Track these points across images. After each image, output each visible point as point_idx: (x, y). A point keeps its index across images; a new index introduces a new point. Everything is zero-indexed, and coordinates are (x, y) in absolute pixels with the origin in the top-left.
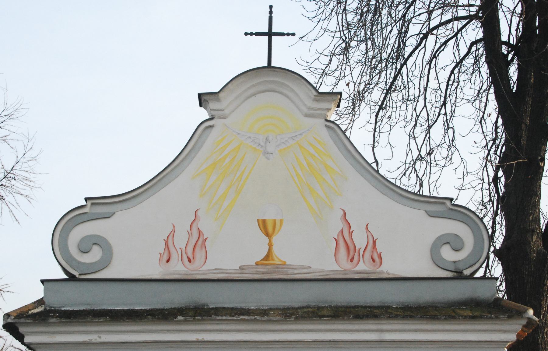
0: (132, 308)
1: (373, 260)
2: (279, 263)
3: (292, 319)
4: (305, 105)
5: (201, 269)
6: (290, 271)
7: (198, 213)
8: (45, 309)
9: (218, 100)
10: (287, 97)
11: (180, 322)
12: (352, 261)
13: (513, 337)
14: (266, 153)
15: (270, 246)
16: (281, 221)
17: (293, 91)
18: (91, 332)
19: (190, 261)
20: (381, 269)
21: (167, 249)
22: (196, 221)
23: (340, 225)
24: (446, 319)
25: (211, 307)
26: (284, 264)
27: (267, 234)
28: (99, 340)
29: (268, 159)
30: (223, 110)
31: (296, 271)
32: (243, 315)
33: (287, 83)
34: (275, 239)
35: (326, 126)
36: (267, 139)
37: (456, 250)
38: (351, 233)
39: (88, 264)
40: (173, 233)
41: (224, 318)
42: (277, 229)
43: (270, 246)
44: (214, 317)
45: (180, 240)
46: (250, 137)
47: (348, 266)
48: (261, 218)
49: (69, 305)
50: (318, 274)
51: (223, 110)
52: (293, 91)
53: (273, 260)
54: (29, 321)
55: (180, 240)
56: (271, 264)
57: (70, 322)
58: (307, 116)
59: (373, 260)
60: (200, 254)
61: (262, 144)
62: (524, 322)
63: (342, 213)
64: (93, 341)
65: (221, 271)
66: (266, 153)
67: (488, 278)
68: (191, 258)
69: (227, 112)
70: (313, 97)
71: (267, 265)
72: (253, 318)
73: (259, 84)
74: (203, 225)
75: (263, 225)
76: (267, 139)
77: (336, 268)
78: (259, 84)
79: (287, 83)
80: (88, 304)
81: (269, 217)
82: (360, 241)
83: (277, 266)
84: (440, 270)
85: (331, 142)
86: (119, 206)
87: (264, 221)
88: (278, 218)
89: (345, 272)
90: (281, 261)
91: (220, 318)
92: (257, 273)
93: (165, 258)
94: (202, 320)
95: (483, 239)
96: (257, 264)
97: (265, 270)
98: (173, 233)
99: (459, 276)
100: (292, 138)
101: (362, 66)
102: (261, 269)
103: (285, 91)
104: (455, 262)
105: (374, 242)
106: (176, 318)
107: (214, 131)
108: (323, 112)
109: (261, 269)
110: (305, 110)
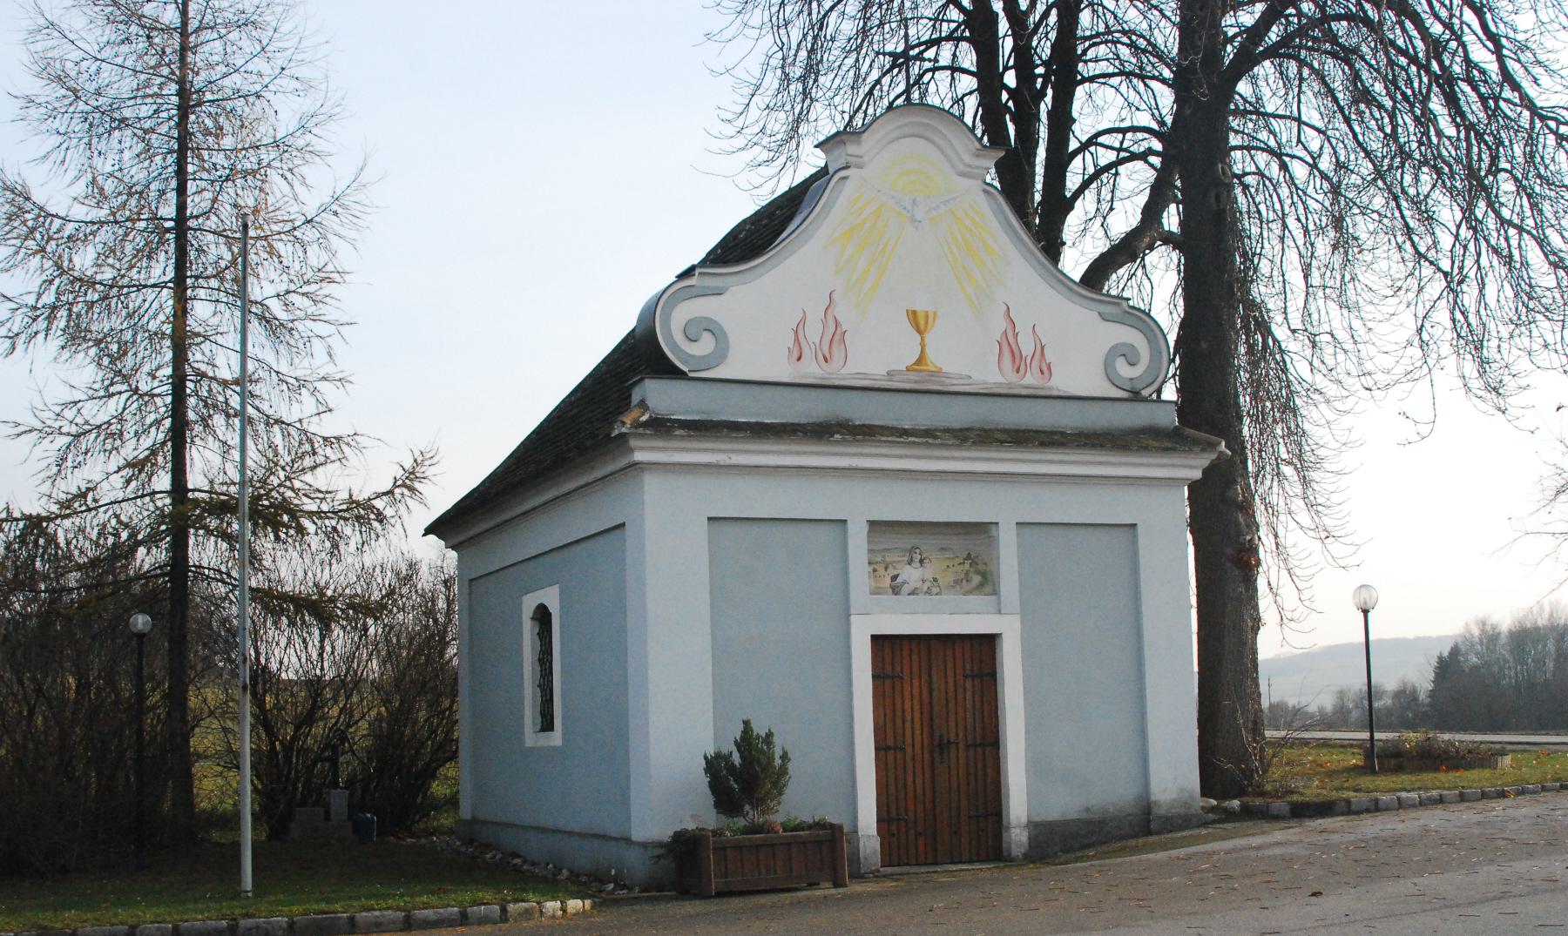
0: (760, 420)
1: (1042, 373)
2: (934, 369)
3: (969, 443)
4: (962, 160)
5: (842, 372)
6: (948, 381)
7: (834, 295)
8: (651, 416)
9: (859, 143)
10: (933, 142)
11: (838, 442)
12: (1018, 371)
13: (1197, 474)
14: (914, 220)
15: (923, 346)
16: (935, 313)
17: (945, 137)
18: (719, 451)
19: (826, 361)
20: (1049, 384)
21: (797, 345)
22: (832, 306)
23: (1000, 325)
24: (1137, 450)
25: (857, 423)
26: (940, 371)
27: (919, 331)
28: (728, 462)
29: (917, 229)
30: (861, 157)
31: (954, 382)
32: (912, 436)
33: (940, 127)
34: (928, 337)
35: (984, 190)
36: (914, 202)
37: (1132, 364)
38: (1016, 335)
39: (699, 357)
40: (803, 320)
41: (890, 439)
42: (929, 327)
43: (923, 346)
44: (879, 437)
45: (813, 332)
46: (894, 198)
47: (1013, 377)
48: (911, 308)
49: (680, 414)
50: (980, 386)
51: (861, 157)
52: (945, 137)
53: (927, 365)
54: (648, 432)
55: (813, 332)
56: (925, 371)
57: (700, 436)
58: (962, 174)
59: (1042, 373)
60: (838, 353)
61: (909, 207)
62: (1214, 456)
63: (1005, 308)
64: (722, 463)
65: (864, 376)
66: (914, 220)
67: (1153, 401)
68: (827, 356)
69: (866, 159)
70: (974, 150)
71: (921, 371)
72: (924, 440)
73: (906, 125)
74: (840, 312)
75: (913, 316)
76: (914, 202)
77: (1001, 380)
78: (906, 125)
79: (945, 131)
80: (703, 413)
81: (920, 308)
82: (1027, 346)
83: (932, 374)
84: (1115, 389)
85: (990, 214)
86: (735, 278)
87: (914, 312)
88: (931, 310)
89: (1010, 385)
90: (936, 367)
91: (885, 438)
92: (909, 381)
93: (796, 355)
94: (864, 440)
95: (1160, 353)
96: (908, 369)
97: (917, 378)
98: (803, 320)
99: (1135, 396)
100: (944, 202)
101: (1412, 307)
102: (912, 376)
103: (936, 139)
104: (1131, 379)
105: (1042, 348)
106: (832, 436)
107: (849, 183)
108: (981, 171)
109: (912, 376)
110: (961, 167)
